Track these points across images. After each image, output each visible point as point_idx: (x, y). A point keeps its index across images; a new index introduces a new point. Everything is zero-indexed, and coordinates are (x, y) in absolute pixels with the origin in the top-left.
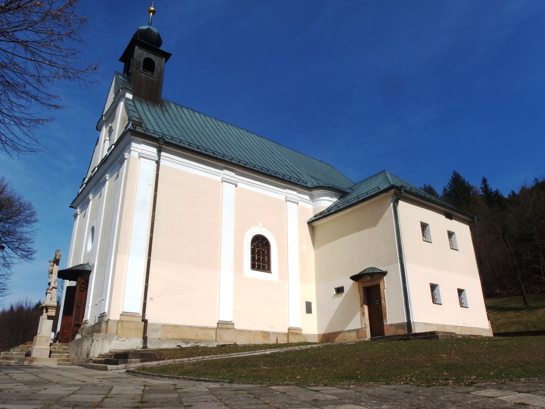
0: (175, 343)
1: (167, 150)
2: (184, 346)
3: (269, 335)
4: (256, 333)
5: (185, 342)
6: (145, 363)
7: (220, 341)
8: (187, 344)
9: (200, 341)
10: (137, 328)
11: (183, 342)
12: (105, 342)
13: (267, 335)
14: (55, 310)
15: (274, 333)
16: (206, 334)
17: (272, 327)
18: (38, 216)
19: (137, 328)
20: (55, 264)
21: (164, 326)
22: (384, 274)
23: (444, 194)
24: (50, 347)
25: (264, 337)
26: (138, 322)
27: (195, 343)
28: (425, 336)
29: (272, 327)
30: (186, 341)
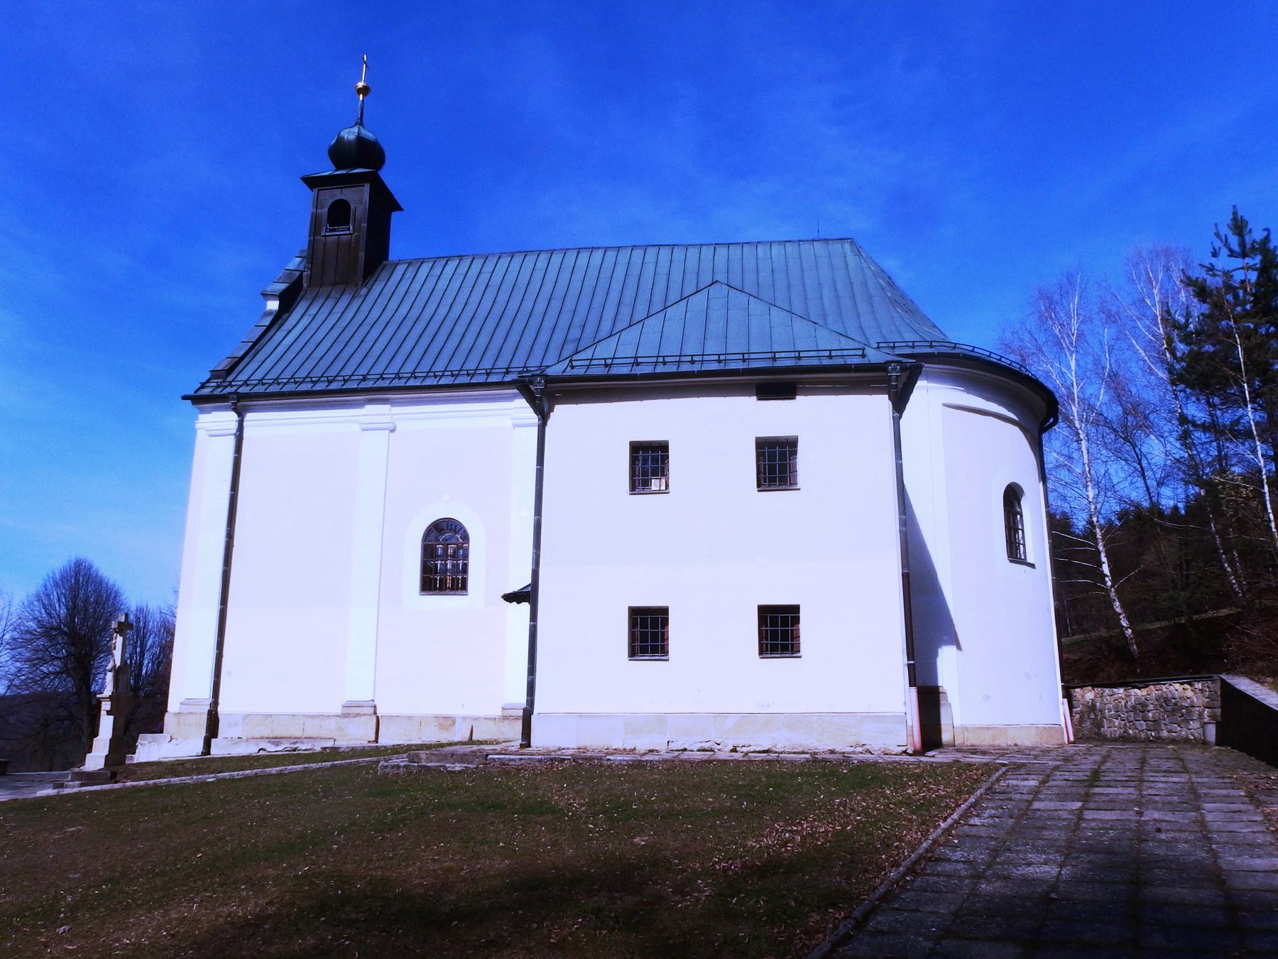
0: (257, 745)
1: (346, 403)
2: (271, 748)
3: (454, 722)
4: (421, 721)
5: (273, 743)
6: (82, 789)
7: (340, 739)
8: (277, 745)
9: (297, 739)
10: (200, 724)
11: (269, 742)
12: (152, 747)
13: (450, 722)
14: (110, 703)
15: (464, 718)
16: (321, 727)
17: (463, 705)
18: (57, 562)
19: (200, 724)
20: (118, 635)
21: (247, 716)
22: (401, 209)
23: (1187, 508)
24: (1067, 694)
25: (441, 727)
26: (201, 713)
27: (291, 744)
28: (306, 765)
29: (463, 705)
30: (276, 740)
